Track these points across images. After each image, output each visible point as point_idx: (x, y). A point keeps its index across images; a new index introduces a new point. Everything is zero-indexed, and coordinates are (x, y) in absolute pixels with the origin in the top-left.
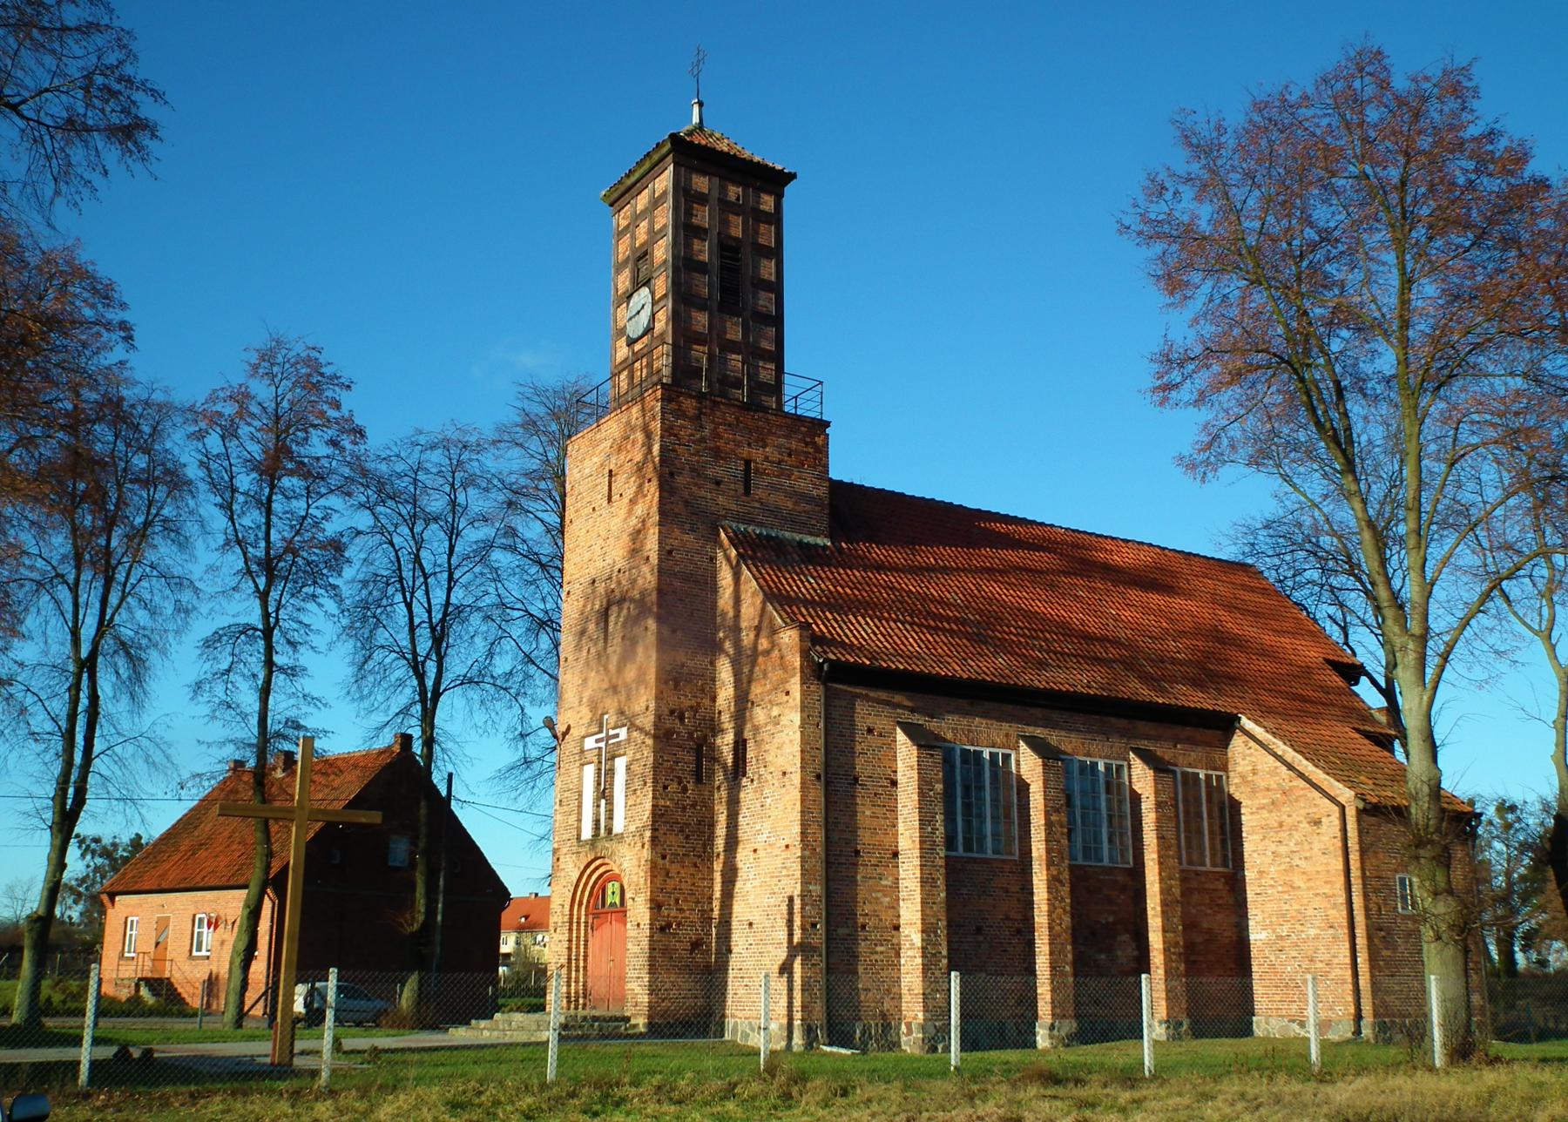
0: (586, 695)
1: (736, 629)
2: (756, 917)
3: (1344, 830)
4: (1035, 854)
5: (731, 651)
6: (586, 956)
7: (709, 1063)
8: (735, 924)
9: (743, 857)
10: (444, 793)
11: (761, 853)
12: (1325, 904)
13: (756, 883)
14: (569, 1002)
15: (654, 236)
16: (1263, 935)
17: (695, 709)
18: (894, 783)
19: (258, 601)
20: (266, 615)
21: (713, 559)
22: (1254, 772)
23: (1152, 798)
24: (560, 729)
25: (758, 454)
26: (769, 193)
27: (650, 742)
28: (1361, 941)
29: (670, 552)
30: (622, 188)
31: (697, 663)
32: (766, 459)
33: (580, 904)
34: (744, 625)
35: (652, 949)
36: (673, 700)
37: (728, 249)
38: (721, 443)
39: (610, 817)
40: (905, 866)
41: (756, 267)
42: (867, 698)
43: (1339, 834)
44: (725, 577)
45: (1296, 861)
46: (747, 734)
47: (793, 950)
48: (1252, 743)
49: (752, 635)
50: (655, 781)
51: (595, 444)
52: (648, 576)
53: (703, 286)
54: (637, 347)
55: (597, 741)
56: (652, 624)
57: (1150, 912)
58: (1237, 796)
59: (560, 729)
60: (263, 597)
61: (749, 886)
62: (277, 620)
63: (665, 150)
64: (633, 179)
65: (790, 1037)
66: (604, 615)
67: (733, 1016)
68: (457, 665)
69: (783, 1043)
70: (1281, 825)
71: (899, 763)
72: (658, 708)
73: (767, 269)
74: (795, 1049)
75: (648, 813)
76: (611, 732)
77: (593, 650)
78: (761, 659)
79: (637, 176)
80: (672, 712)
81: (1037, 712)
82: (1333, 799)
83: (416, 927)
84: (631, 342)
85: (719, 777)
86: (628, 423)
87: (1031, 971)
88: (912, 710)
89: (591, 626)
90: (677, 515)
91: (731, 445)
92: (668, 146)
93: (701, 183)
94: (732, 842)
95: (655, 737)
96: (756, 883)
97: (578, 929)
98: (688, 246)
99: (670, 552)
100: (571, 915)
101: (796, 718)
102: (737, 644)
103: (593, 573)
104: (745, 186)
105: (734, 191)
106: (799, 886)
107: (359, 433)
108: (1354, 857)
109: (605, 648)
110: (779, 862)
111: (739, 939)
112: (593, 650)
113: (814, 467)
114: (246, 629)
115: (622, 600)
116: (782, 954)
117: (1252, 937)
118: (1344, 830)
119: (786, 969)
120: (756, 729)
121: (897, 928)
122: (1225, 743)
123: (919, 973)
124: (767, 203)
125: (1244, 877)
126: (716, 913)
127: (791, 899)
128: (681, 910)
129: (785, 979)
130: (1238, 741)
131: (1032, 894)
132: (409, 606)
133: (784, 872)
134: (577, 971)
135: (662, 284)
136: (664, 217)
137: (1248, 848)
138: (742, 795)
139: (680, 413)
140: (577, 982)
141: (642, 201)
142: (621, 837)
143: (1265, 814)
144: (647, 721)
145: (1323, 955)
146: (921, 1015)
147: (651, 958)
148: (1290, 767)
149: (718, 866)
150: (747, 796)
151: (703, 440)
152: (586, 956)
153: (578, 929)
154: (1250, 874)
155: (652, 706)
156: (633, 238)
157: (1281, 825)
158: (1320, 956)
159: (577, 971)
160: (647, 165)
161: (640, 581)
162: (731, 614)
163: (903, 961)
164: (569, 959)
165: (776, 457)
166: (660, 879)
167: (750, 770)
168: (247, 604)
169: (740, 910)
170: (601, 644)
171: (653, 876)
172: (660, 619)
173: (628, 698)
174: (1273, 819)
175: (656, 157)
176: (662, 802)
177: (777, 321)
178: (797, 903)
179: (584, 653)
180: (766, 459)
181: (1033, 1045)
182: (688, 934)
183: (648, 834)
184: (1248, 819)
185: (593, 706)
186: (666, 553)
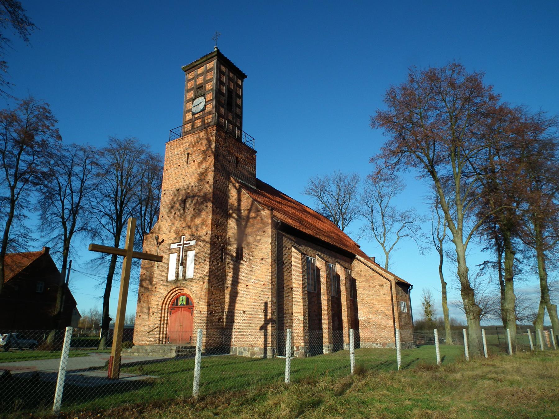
0: (173, 229)
1: (239, 210)
2: (247, 309)
3: (391, 288)
4: (322, 291)
5: (236, 217)
6: (167, 324)
7: (136, 354)
8: (236, 312)
9: (241, 288)
10: (59, 266)
11: (250, 287)
12: (384, 309)
13: (248, 297)
14: (159, 341)
15: (206, 82)
16: (363, 318)
17: (221, 236)
18: (291, 265)
19: (10, 190)
20: (13, 195)
21: (227, 186)
22: (361, 271)
23: (344, 276)
24: (160, 240)
25: (240, 156)
26: (240, 79)
27: (208, 245)
28: (396, 320)
29: (216, 181)
30: (192, 66)
31: (222, 220)
32: (242, 158)
33: (166, 304)
34: (242, 208)
35: (207, 321)
36: (216, 232)
37: (229, 91)
38: (230, 149)
39: (185, 272)
40: (295, 293)
41: (236, 100)
42: (286, 237)
43: (390, 289)
44: (233, 193)
45: (375, 297)
46: (244, 245)
47: (267, 321)
48: (360, 263)
49: (246, 212)
50: (210, 260)
51: (180, 145)
52: (208, 188)
53: (224, 100)
54: (196, 116)
55: (178, 245)
56: (210, 205)
57: (343, 311)
58: (355, 277)
59: (160, 240)
60: (12, 188)
61: (243, 298)
62: (17, 197)
63: (214, 54)
64: (197, 63)
65: (265, 352)
66: (184, 202)
67: (235, 345)
68: (79, 223)
69: (262, 356)
70: (370, 286)
71: (293, 259)
72: (212, 234)
73: (239, 102)
74: (268, 357)
75: (206, 271)
76: (185, 242)
77: (177, 214)
78: (251, 220)
79: (199, 62)
80: (215, 236)
81: (319, 247)
82: (387, 279)
83: (56, 313)
84: (194, 114)
85: (229, 260)
86: (199, 137)
87: (321, 328)
88: (295, 242)
89: (177, 205)
90: (219, 169)
91: (233, 151)
92: (216, 53)
93: (224, 69)
94: (236, 282)
95: (211, 244)
96: (248, 297)
97: (164, 314)
98: (220, 86)
99: (216, 181)
100: (162, 308)
101: (269, 240)
102: (239, 215)
103: (178, 187)
104: (234, 75)
105: (231, 75)
106: (270, 299)
107: (60, 138)
108: (394, 296)
109: (184, 212)
110: (260, 290)
111: (238, 318)
112: (177, 214)
113: (252, 164)
114: (6, 198)
115: (193, 197)
116: (262, 323)
117: (359, 318)
118: (391, 288)
119: (263, 328)
120: (248, 244)
121: (292, 314)
122: (351, 262)
123: (302, 329)
124: (239, 82)
125: (357, 301)
126: (226, 308)
127: (266, 303)
128: (216, 307)
129: (263, 331)
130: (355, 262)
131: (321, 304)
132: (62, 202)
133: (262, 293)
134: (163, 329)
135: (209, 97)
136: (212, 75)
137: (358, 293)
138: (241, 266)
139: (220, 136)
140: (163, 333)
141: (200, 70)
142: (191, 280)
143: (364, 283)
144: (208, 238)
145: (383, 323)
146: (303, 344)
147: (207, 324)
148: (373, 270)
149: (227, 292)
150: (244, 267)
151: (226, 147)
152: (167, 324)
153: (164, 314)
154: (359, 300)
155: (209, 233)
156: (196, 82)
157: (370, 286)
158: (382, 324)
159: (163, 329)
160: (205, 59)
161: (204, 190)
162: (236, 204)
163: (294, 325)
164: (160, 325)
165: (244, 158)
166: (210, 295)
167: (244, 258)
168: (4, 190)
169: (239, 307)
170: (182, 212)
171: (208, 294)
172: (213, 203)
173: (197, 230)
174: (367, 284)
175: (209, 57)
176: (212, 267)
177: (241, 118)
178: (269, 305)
179: (173, 214)
180: (242, 158)
181: (322, 353)
182: (218, 315)
183: (207, 278)
184: (358, 284)
185: (177, 232)
186: (215, 181)
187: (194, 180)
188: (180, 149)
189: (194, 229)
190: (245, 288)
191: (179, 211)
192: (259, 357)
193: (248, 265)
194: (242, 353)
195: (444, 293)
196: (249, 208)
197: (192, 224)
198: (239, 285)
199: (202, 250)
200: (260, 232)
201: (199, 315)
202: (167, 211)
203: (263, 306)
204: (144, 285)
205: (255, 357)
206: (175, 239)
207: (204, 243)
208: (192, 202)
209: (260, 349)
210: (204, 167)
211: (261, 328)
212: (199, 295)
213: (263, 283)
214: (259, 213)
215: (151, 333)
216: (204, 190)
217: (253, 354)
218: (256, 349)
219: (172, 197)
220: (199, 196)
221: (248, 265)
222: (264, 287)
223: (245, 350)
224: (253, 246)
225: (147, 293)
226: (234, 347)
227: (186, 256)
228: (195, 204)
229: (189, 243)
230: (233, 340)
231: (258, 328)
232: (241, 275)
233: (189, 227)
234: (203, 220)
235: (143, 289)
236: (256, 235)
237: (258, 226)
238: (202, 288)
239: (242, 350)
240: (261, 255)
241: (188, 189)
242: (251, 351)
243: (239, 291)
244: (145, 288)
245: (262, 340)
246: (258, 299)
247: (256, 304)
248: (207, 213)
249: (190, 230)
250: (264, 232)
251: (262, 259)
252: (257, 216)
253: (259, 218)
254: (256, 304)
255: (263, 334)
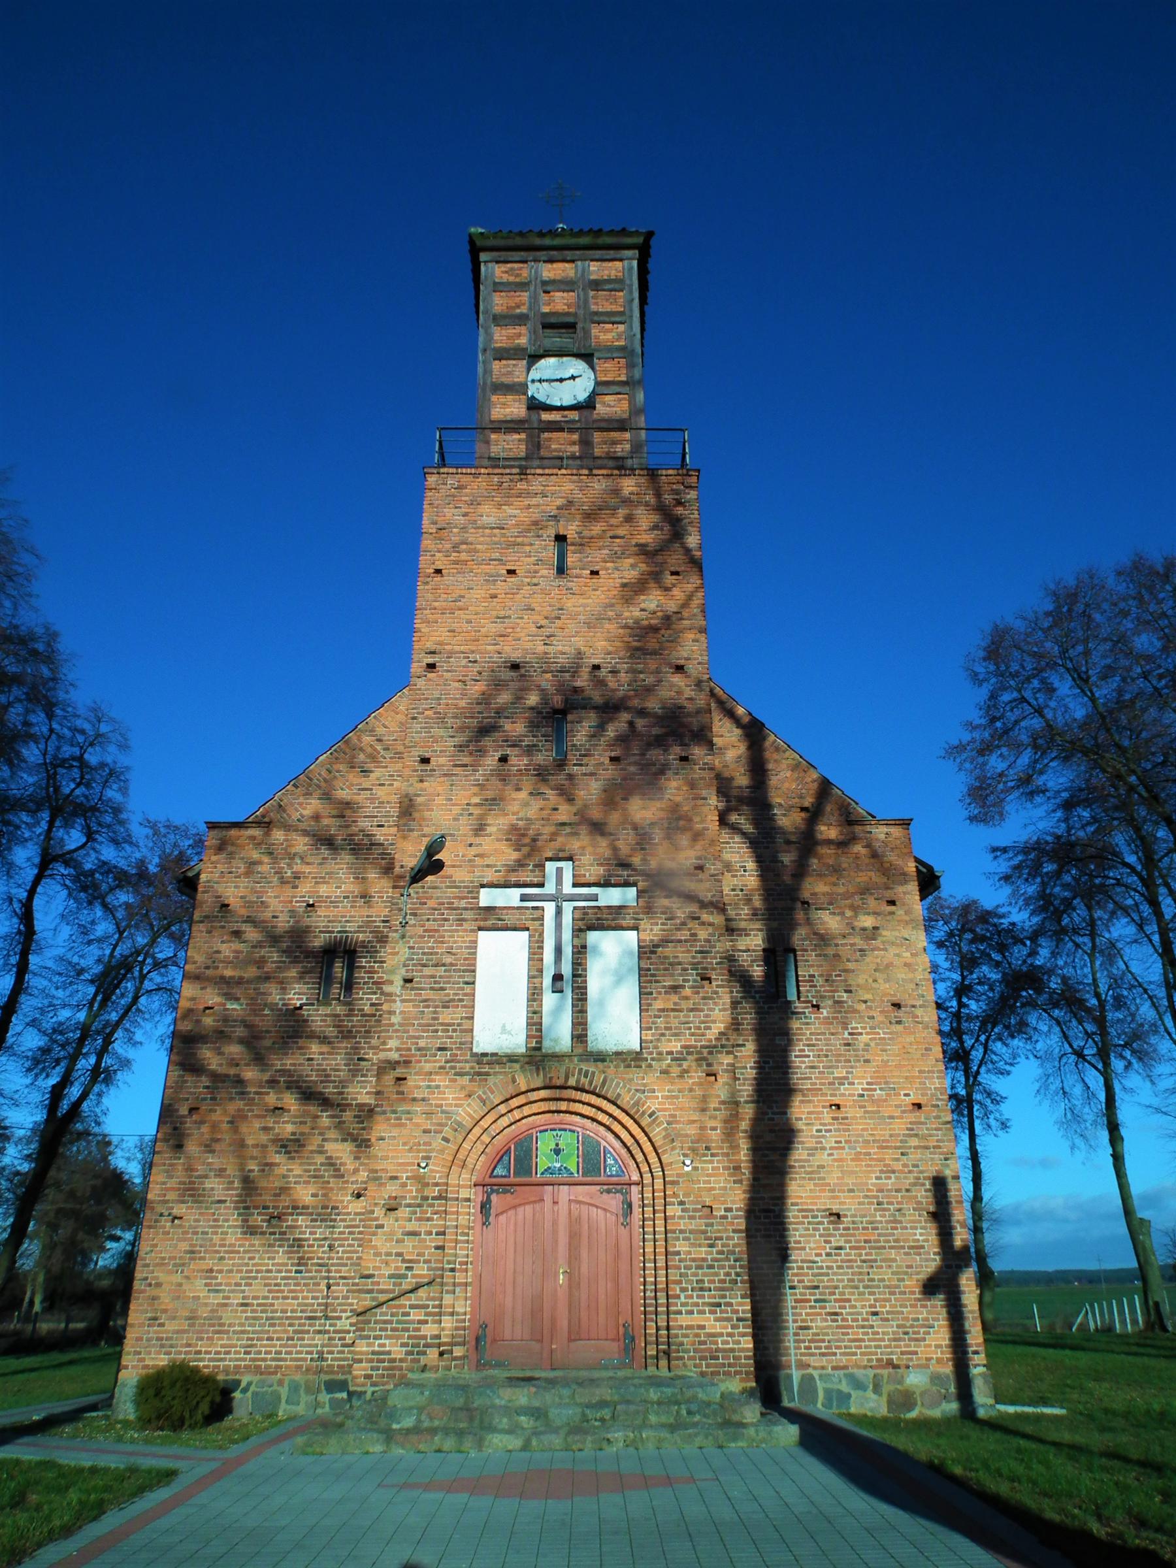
2: (848, 1205)
5: (748, 828)
8: (793, 1214)
11: (849, 1112)
30: (519, 241)
34: (776, 799)
46: (799, 938)
61: (823, 1158)
64: (547, 241)
67: (802, 1365)
79: (557, 242)
89: (516, 728)
96: (846, 1153)
110: (899, 1127)
112: (518, 761)
116: (930, 1261)
127: (939, 1185)
129: (938, 1303)
138: (795, 1025)
179: (491, 760)
187: (601, 644)
188: (510, 511)
189: (625, 842)
190: (827, 1115)
191: (530, 750)
192: (936, 1413)
193: (827, 1021)
194: (844, 1398)
195: (771, 1147)
196: (808, 802)
197: (614, 818)
198: (797, 1100)
199: (684, 935)
200: (872, 903)
201: (698, 1224)
202: (451, 743)
203: (924, 1195)
204: (209, 1057)
205: (913, 1414)
206: (512, 870)
207: (693, 908)
208: (601, 727)
209: (936, 1378)
210: (652, 606)
211: (931, 1287)
212: (692, 1130)
213: (913, 1098)
214: (858, 829)
215: (381, 1314)
216: (665, 693)
217: (906, 1400)
218: (915, 1380)
219: (480, 687)
220: (642, 713)
221: (827, 1021)
222: (921, 1116)
223: (859, 1385)
224: (845, 952)
225: (233, 1107)
226: (796, 1375)
227: (581, 951)
228: (623, 740)
229: (595, 898)
230: (790, 1342)
231: (913, 1284)
232: (805, 1061)
233: (598, 828)
234: (674, 808)
235: (197, 1086)
236: (855, 909)
237: (862, 878)
238: (705, 1099)
239: (844, 1387)
240: (887, 989)
241: (575, 671)
242: (886, 1388)
243: (800, 1125)
244: (216, 1078)
245: (940, 1336)
246: (898, 1166)
247: (890, 1183)
248: (692, 785)
249: (603, 843)
250: (892, 903)
251: (897, 1006)
252: (852, 839)
253: (858, 848)
254: (890, 1183)
255: (943, 1313)
